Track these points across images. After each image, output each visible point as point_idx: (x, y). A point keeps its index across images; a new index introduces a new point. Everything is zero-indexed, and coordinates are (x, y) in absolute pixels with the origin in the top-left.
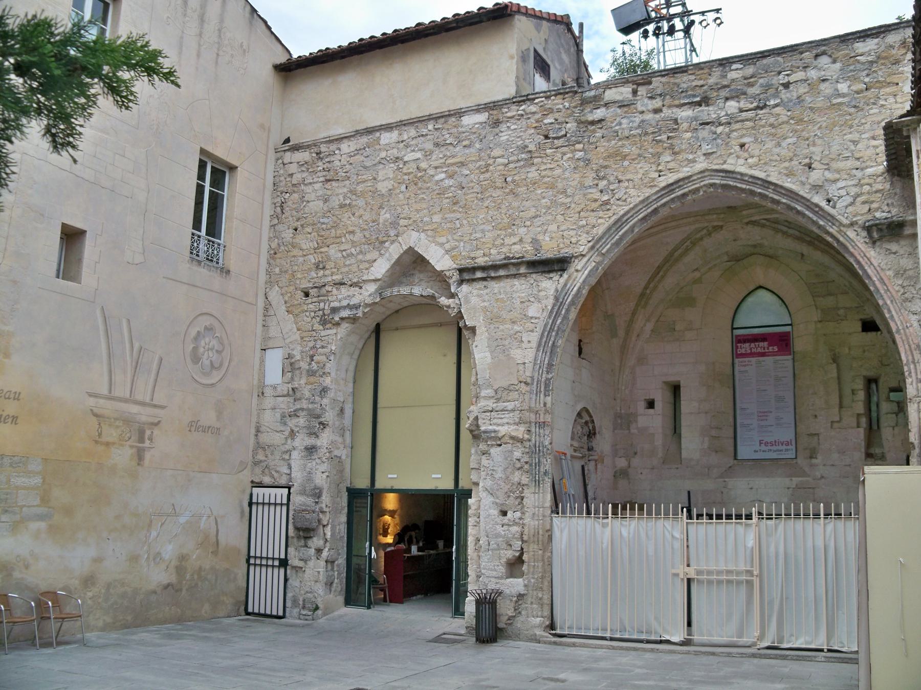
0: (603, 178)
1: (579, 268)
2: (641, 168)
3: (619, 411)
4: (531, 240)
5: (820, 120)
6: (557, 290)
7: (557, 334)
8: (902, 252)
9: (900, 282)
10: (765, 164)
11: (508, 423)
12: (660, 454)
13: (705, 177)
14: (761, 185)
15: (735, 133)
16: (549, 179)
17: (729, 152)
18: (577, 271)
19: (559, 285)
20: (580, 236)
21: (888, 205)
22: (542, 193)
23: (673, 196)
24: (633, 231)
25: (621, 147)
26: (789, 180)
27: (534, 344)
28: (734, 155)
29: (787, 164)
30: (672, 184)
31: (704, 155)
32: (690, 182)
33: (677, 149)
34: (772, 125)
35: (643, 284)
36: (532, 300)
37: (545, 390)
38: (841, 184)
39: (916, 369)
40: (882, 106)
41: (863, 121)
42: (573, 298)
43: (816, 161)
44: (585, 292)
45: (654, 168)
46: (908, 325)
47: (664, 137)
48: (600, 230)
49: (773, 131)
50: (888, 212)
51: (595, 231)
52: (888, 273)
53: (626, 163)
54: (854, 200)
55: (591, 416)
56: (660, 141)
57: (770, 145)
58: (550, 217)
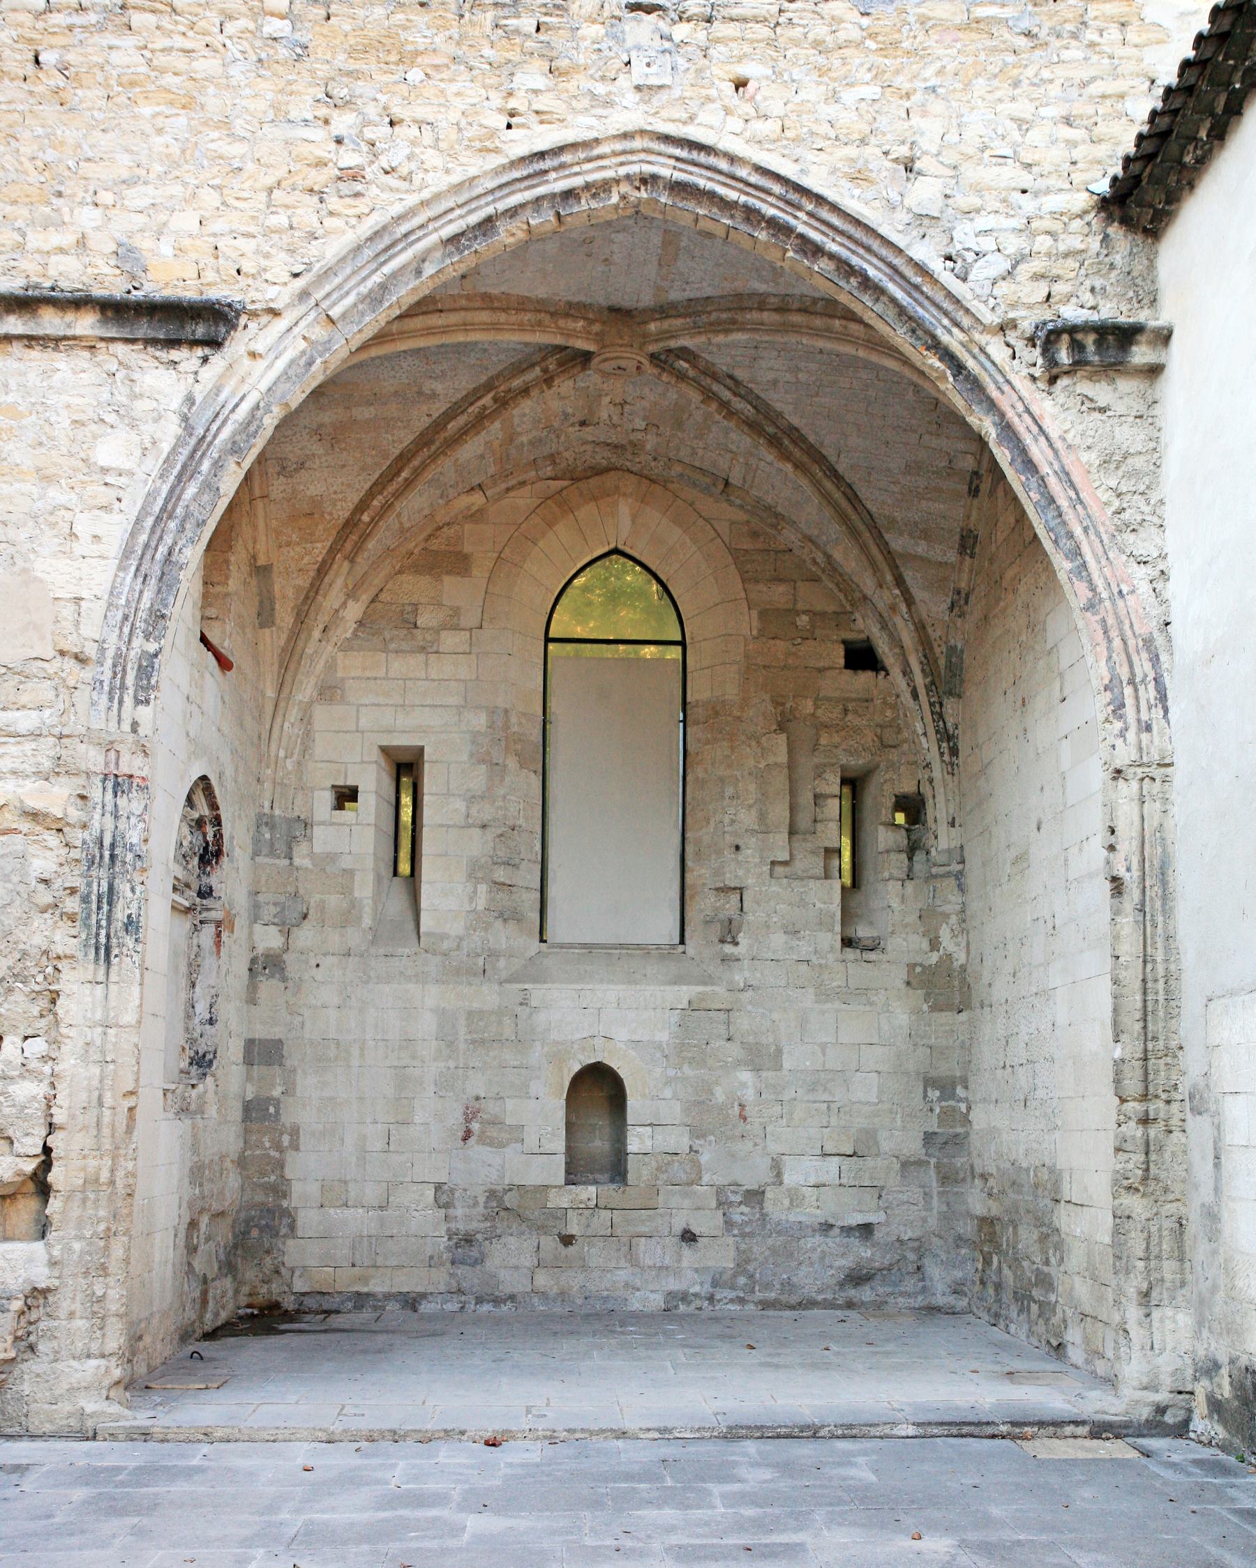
0: (346, 104)
1: (259, 347)
2: (458, 94)
3: (267, 810)
4: (114, 247)
5: (941, 52)
6: (190, 400)
7: (181, 529)
8: (1120, 408)
9: (1113, 483)
10: (797, 140)
11: (14, 773)
12: (367, 921)
13: (632, 152)
14: (779, 198)
15: (721, 48)
16: (177, 80)
17: (704, 92)
18: (253, 355)
19: (198, 387)
20: (267, 256)
21: (1093, 290)
22: (154, 116)
23: (541, 190)
24: (419, 272)
25: (405, 28)
26: (857, 192)
27: (114, 547)
28: (717, 105)
29: (852, 151)
30: (541, 155)
31: (638, 88)
32: (590, 160)
33: (563, 63)
34: (817, 44)
35: (355, 498)
36: (111, 418)
37: (138, 687)
38: (983, 222)
39: (1137, 698)
40: (1092, 45)
41: (1046, 74)
42: (234, 434)
43: (925, 153)
44: (270, 422)
45: (497, 100)
46: (1125, 589)
47: (528, 24)
48: (332, 249)
49: (821, 60)
50: (1093, 308)
51: (314, 248)
52: (1085, 457)
53: (415, 75)
54: (1014, 267)
55: (214, 806)
56: (517, 31)
57: (812, 92)
58: (177, 189)
